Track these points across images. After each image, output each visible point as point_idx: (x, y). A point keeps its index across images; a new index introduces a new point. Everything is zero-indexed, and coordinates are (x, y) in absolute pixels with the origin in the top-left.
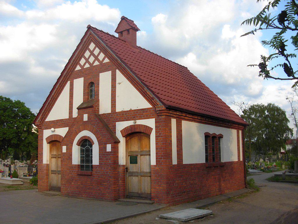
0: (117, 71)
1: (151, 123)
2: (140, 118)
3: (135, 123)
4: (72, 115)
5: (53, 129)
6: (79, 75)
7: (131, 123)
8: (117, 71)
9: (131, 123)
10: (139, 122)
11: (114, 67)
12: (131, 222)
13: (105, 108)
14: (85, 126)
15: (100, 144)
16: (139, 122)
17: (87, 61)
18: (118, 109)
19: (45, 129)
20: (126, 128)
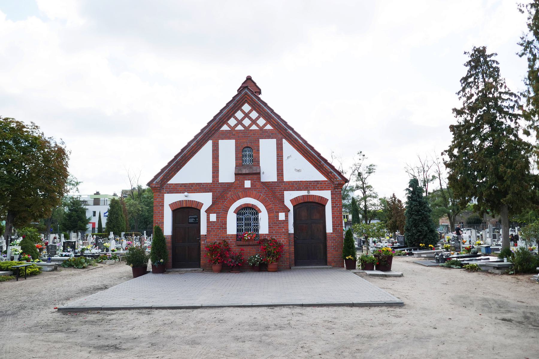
0: (284, 140)
1: (327, 194)
2: (314, 189)
3: (448, 228)
4: (288, 190)
5: (186, 194)
6: (227, 136)
7: (305, 193)
8: (284, 140)
9: (305, 193)
10: (313, 193)
11: (280, 136)
12: (315, 319)
13: (269, 174)
14: (247, 193)
15: (269, 211)
16: (313, 193)
17: (240, 122)
18: (286, 179)
19: (168, 193)
20: (297, 198)
